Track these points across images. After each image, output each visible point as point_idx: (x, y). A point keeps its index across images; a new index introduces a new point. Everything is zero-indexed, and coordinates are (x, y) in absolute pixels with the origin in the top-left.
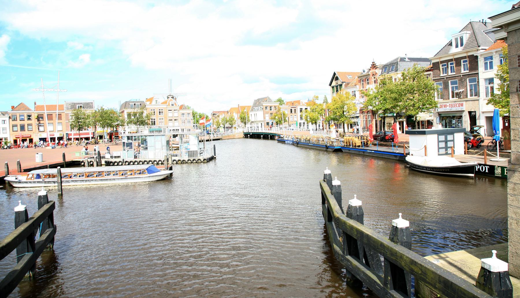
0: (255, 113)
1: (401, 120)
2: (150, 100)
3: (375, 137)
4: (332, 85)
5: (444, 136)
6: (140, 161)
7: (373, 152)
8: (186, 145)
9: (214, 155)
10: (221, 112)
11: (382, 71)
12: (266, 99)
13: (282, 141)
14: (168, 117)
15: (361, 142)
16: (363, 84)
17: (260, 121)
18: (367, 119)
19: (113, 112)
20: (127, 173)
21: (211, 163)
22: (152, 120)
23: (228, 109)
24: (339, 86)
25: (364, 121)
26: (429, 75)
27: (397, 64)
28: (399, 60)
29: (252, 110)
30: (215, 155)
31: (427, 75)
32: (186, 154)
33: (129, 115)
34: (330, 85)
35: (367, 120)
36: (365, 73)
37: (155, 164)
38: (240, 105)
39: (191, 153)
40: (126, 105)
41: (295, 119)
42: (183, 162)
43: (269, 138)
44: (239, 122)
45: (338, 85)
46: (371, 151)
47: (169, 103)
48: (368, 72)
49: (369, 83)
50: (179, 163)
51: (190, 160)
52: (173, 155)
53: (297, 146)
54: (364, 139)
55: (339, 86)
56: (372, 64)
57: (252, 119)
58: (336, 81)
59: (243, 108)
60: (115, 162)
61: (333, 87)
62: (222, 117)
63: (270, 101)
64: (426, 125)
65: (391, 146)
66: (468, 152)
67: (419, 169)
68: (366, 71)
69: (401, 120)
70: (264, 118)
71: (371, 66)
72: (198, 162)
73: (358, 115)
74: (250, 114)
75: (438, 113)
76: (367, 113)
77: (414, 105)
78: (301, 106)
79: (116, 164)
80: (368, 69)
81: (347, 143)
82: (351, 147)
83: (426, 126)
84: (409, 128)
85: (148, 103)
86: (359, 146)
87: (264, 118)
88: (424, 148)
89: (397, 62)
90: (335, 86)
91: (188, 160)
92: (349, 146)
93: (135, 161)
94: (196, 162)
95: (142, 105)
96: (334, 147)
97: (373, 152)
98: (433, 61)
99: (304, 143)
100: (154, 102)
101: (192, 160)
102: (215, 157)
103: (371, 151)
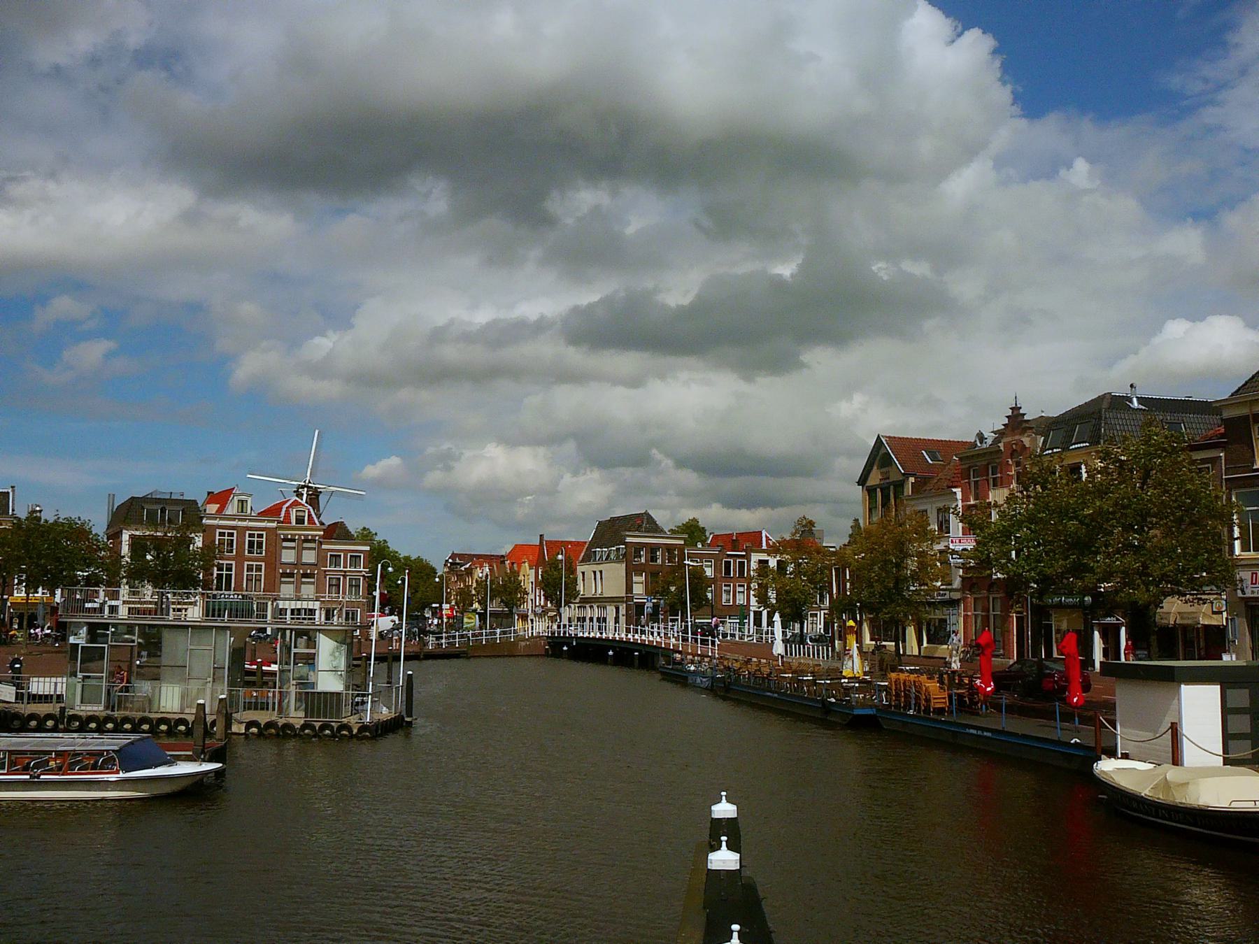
0: (597, 568)
1: (1109, 620)
2: (221, 498)
3: (1003, 680)
4: (870, 483)
5: (1247, 691)
6: (126, 720)
7: (989, 734)
8: (302, 669)
9: (404, 713)
10: (479, 556)
11: (1045, 442)
12: (643, 522)
13: (678, 677)
14: (278, 563)
15: (950, 696)
16: (976, 482)
17: (612, 600)
18: (989, 612)
19: (77, 532)
20: (47, 762)
21: (392, 742)
22: (220, 569)
23: (506, 550)
24: (892, 487)
25: (976, 616)
26: (1214, 461)
27: (1100, 418)
28: (1105, 405)
29: (588, 558)
30: (410, 715)
31: (1204, 461)
32: (298, 704)
33: (138, 546)
34: (862, 481)
35: (988, 617)
36: (984, 446)
37: (162, 732)
38: (545, 538)
39: (316, 702)
40: (128, 512)
41: (741, 600)
42: (285, 733)
43: (637, 662)
44: (534, 599)
45: (890, 484)
46: (980, 733)
47: (287, 512)
48: (996, 441)
49: (999, 480)
50: (271, 734)
51: (331, 728)
52: (256, 703)
53: (724, 699)
54: (960, 685)
55: (892, 487)
56: (1010, 412)
57: (586, 588)
58: (884, 470)
59: (556, 546)
60: (32, 716)
61: (871, 491)
62: (481, 572)
63: (653, 528)
64: (1202, 644)
65: (1050, 715)
66: (264, 592)
67: (1135, 810)
68: (990, 437)
69: (1109, 620)
70: (629, 588)
71: (1006, 421)
72: (342, 735)
73: (957, 596)
74: (580, 569)
75: (1246, 600)
76: (989, 591)
77: (1144, 572)
78: (763, 551)
79: (33, 723)
80: (995, 432)
81: (897, 695)
82: (911, 712)
83: (1199, 650)
84: (1138, 652)
85: (213, 508)
86: (940, 711)
87: (629, 588)
88: (1168, 736)
89: (1100, 412)
90: (878, 486)
91: (304, 727)
92: (904, 708)
93: (108, 719)
94: (333, 736)
95: (190, 513)
96: (852, 708)
97: (989, 734)
98: (1226, 414)
99: (749, 687)
100: (232, 509)
101: (317, 725)
102: (408, 719)
103: (980, 733)
